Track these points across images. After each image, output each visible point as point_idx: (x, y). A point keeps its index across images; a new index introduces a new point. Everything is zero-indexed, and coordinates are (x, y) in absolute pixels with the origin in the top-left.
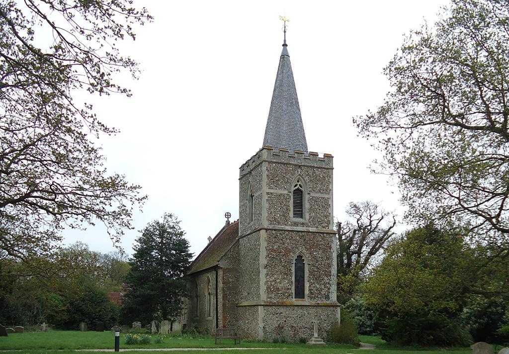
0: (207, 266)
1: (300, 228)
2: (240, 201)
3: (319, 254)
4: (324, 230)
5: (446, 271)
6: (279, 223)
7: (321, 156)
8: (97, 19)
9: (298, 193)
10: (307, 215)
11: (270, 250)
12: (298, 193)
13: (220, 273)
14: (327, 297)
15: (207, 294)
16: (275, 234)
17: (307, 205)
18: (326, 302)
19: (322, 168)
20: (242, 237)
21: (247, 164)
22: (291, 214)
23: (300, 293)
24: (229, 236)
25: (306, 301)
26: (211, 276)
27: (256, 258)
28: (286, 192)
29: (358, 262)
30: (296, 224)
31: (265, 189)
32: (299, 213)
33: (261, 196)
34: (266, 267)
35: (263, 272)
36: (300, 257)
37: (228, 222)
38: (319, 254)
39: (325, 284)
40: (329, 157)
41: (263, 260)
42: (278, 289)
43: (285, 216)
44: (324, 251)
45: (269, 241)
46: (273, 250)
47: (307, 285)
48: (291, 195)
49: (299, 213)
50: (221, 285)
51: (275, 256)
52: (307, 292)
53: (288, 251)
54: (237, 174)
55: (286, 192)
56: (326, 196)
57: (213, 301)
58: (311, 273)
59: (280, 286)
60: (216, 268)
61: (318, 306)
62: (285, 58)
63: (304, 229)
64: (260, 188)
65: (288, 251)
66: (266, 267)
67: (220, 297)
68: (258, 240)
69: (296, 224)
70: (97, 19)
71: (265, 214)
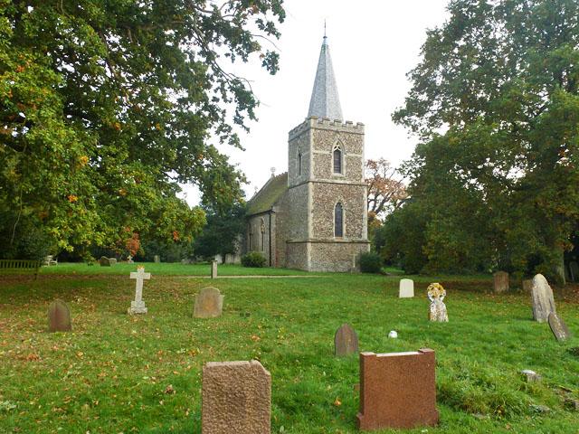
0: (261, 210)
1: (338, 181)
2: (289, 159)
3: (353, 201)
4: (357, 183)
5: (267, 369)
6: (322, 177)
7: (355, 124)
8: (233, 60)
9: (338, 153)
10: (344, 171)
11: (316, 198)
12: (338, 153)
13: (274, 216)
14: (360, 236)
15: (260, 234)
16: (321, 185)
17: (344, 163)
18: (359, 239)
19: (354, 134)
20: (291, 188)
21: (295, 130)
22: (332, 169)
23: (339, 233)
24: (277, 183)
25: (345, 239)
26: (265, 218)
27: (305, 204)
28: (328, 152)
29: (375, 207)
30: (336, 178)
31: (312, 150)
32: (338, 169)
33: (309, 156)
34: (312, 212)
35: (311, 215)
36: (339, 203)
37: (273, 175)
38: (353, 201)
39: (358, 225)
40: (360, 125)
41: (311, 206)
42: (322, 230)
43: (327, 171)
44: (358, 199)
45: (315, 191)
46: (318, 198)
47: (344, 226)
48: (332, 154)
49: (338, 169)
50: (274, 226)
51: (321, 202)
52: (344, 232)
53: (330, 199)
54: (286, 137)
55: (328, 152)
56: (359, 156)
57: (267, 237)
58: (347, 217)
59: (323, 227)
60: (270, 212)
61: (353, 242)
62: (324, 47)
63: (342, 182)
64: (308, 149)
65: (330, 199)
66: (312, 212)
67: (273, 235)
68: (307, 189)
69: (336, 178)
70: (233, 60)
71: (312, 170)
